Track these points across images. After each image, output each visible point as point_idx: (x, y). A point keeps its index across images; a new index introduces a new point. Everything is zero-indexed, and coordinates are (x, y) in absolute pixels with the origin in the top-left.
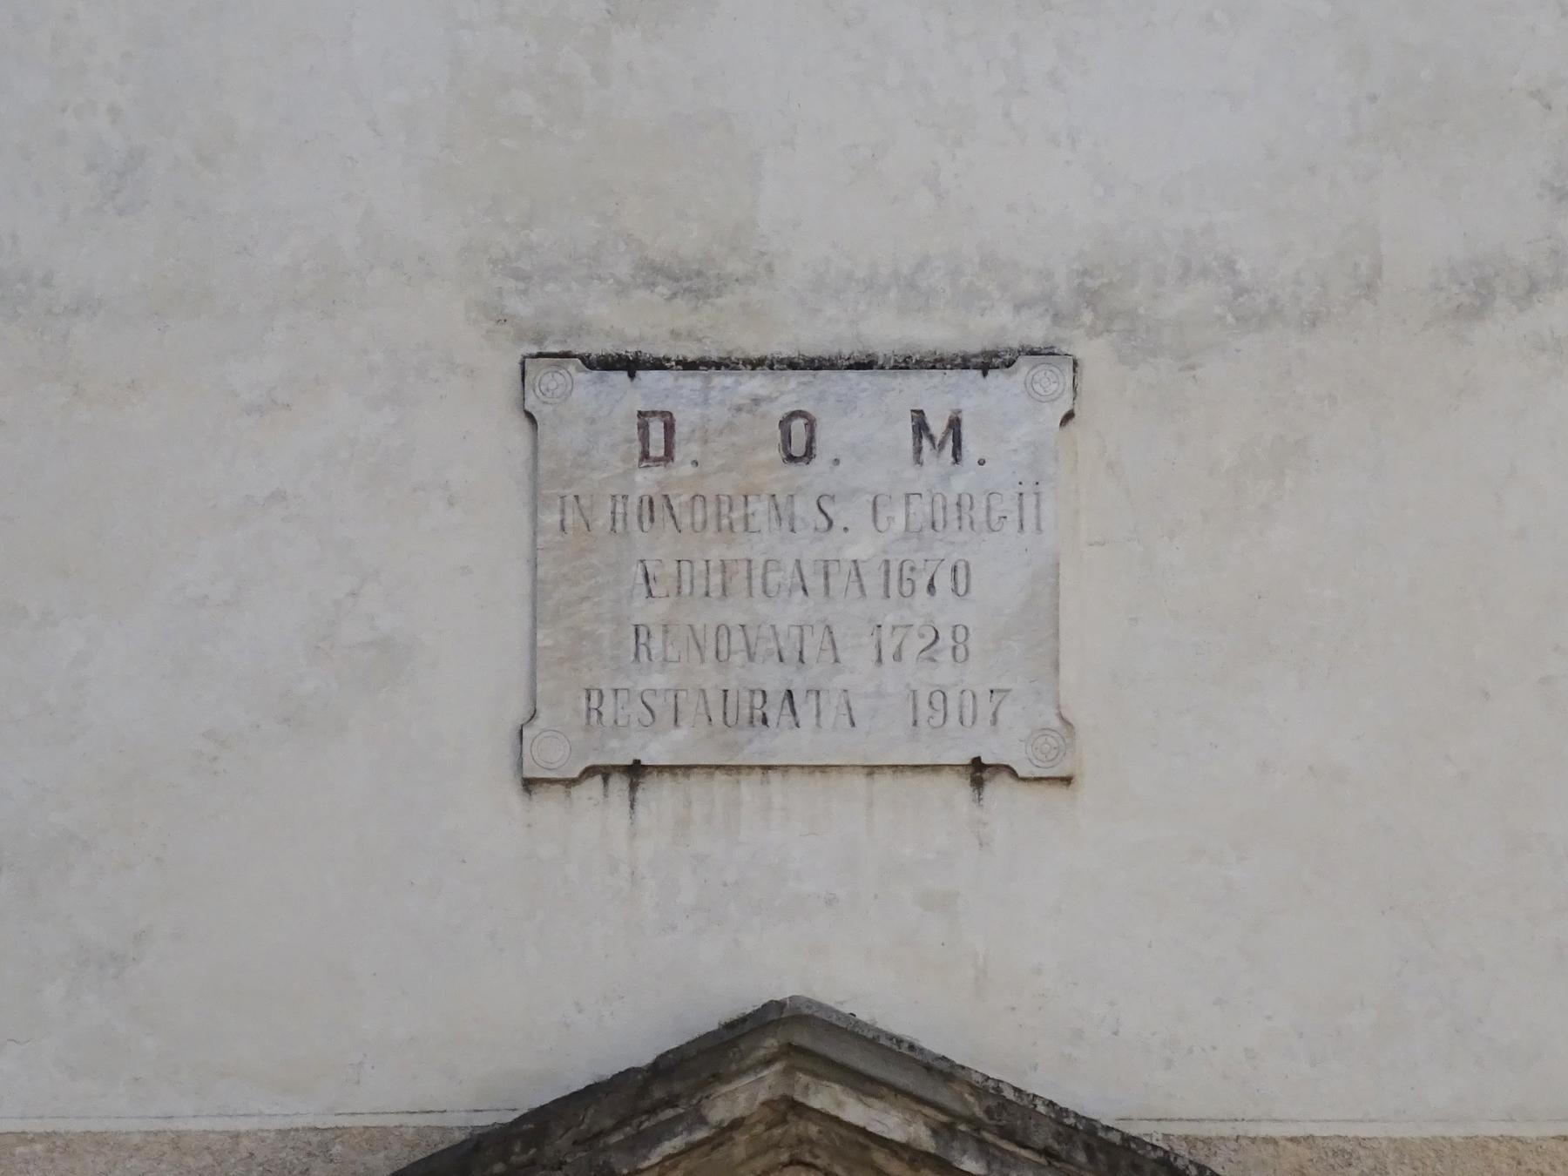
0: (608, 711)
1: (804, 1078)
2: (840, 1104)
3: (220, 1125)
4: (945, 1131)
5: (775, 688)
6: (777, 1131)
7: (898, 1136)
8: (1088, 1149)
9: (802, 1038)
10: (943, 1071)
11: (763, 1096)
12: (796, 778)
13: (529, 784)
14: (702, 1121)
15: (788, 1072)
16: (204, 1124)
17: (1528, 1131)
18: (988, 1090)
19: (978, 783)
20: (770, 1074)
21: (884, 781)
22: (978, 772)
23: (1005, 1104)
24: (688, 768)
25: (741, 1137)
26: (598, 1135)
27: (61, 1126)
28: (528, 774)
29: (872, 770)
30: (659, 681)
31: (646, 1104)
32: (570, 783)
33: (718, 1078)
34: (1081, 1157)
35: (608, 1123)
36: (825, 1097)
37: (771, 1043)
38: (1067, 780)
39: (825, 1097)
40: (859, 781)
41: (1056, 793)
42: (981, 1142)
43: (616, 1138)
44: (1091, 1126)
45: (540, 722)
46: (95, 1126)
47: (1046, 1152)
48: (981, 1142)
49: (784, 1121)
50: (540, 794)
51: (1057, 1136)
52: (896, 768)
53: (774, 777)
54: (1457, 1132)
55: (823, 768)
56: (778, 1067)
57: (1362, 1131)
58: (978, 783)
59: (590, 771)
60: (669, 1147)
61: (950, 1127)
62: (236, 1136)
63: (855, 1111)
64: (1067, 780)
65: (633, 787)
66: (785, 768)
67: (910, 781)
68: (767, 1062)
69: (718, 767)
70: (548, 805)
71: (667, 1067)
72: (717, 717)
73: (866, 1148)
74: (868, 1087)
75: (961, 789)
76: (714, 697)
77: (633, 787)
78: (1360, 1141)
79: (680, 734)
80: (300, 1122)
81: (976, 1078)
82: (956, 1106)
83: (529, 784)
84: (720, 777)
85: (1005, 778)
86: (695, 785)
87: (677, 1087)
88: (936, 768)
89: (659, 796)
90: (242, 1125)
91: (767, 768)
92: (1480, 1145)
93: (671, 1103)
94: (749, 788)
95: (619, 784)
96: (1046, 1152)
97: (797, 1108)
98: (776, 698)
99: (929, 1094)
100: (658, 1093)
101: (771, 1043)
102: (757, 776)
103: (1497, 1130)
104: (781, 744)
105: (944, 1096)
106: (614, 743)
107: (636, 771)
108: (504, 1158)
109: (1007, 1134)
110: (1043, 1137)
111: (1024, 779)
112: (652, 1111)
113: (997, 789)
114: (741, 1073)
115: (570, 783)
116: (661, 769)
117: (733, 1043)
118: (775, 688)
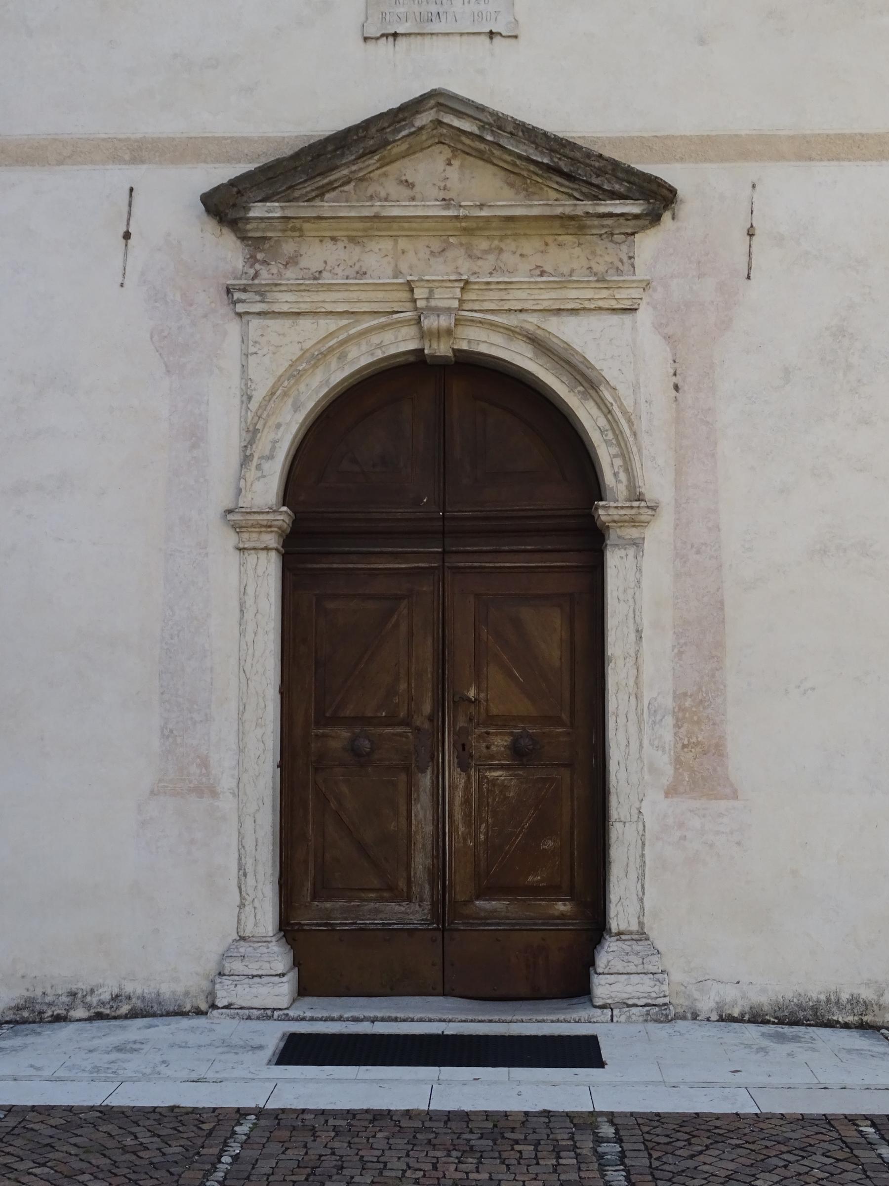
0: (387, 18)
1: (442, 113)
2: (452, 121)
3: (279, 134)
4: (482, 128)
5: (434, 11)
6: (435, 132)
7: (469, 130)
8: (523, 131)
9: (442, 101)
10: (481, 109)
11: (430, 119)
12: (440, 37)
13: (366, 39)
14: (413, 126)
15: (437, 112)
16: (275, 134)
17: (645, 135)
18: (494, 114)
19: (491, 38)
20: (432, 112)
21: (465, 37)
22: (491, 34)
23: (499, 118)
24: (410, 34)
25: (424, 132)
26: (384, 128)
27: (235, 135)
28: (365, 35)
29: (462, 34)
30: (402, 10)
31: (397, 119)
32: (377, 39)
33: (418, 112)
34: (520, 134)
35: (386, 125)
36: (449, 119)
37: (432, 102)
38: (516, 37)
39: (449, 119)
40: (458, 38)
41: (513, 41)
42: (492, 131)
43: (388, 130)
44: (524, 124)
45: (369, 21)
46: (245, 135)
47: (511, 133)
48: (492, 131)
49: (436, 128)
50: (369, 42)
51: (514, 128)
52: (468, 34)
53: (434, 37)
54: (625, 135)
55: (448, 34)
56: (435, 110)
57: (599, 135)
58: (491, 38)
59: (383, 35)
60: (404, 133)
61: (483, 127)
62: (284, 138)
63: (456, 123)
64: (516, 37)
65: (395, 40)
66: (437, 34)
67: (472, 38)
68: (432, 108)
69: (419, 34)
70: (371, 45)
71: (403, 108)
72: (418, 20)
73: (459, 136)
74: (461, 115)
75: (485, 40)
76: (417, 14)
77: (395, 40)
78: (598, 138)
79: (408, 24)
80: (302, 134)
81: (491, 111)
82: (485, 120)
83: (366, 39)
84: (419, 37)
85: (499, 37)
86: (412, 39)
87: (406, 114)
88: (479, 34)
89: (402, 42)
90: (286, 135)
91: (432, 34)
92: (632, 139)
93: (404, 120)
94: (427, 39)
95: (391, 39)
96: (511, 133)
97: (440, 123)
98: (435, 14)
99: (478, 116)
100: (401, 116)
101: (432, 102)
102: (429, 36)
103: (636, 134)
104: (436, 27)
105: (481, 117)
106: (389, 27)
107: (395, 35)
108: (357, 135)
109: (500, 128)
110: (510, 128)
111: (504, 37)
112: (399, 122)
113: (497, 40)
114: (424, 111)
115: (377, 39)
116: (403, 35)
117: (424, 99)
118: (434, 11)
